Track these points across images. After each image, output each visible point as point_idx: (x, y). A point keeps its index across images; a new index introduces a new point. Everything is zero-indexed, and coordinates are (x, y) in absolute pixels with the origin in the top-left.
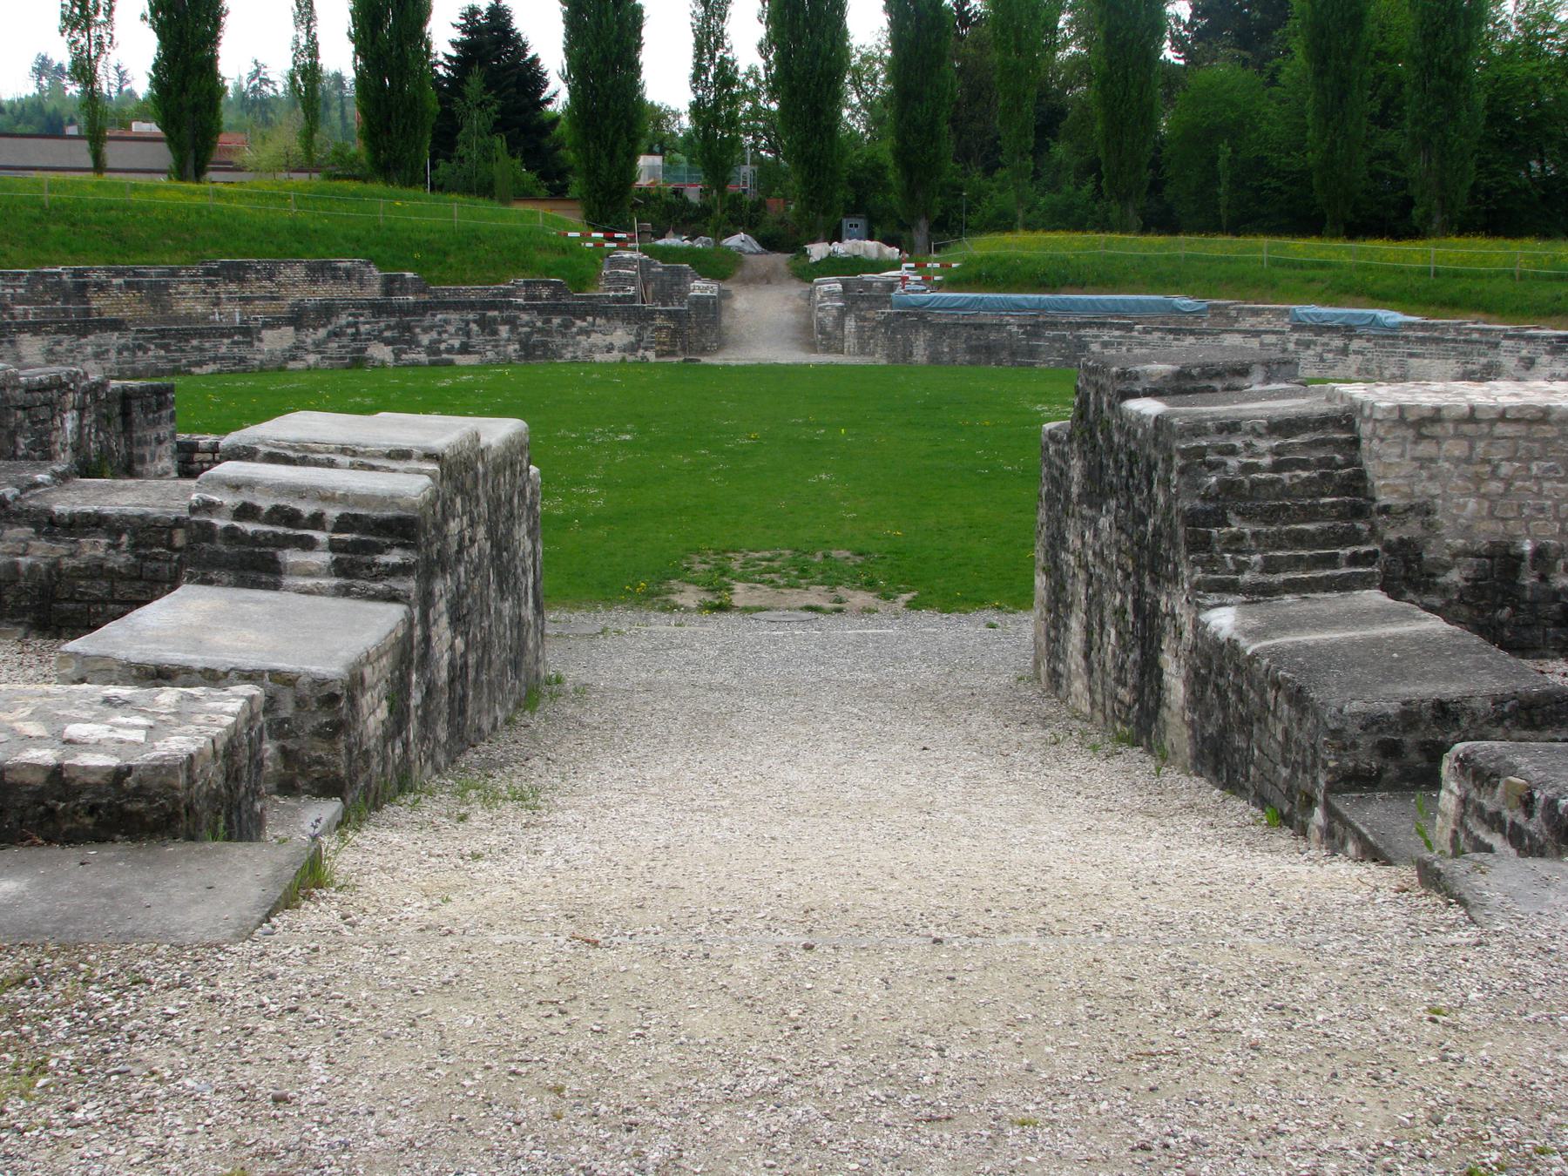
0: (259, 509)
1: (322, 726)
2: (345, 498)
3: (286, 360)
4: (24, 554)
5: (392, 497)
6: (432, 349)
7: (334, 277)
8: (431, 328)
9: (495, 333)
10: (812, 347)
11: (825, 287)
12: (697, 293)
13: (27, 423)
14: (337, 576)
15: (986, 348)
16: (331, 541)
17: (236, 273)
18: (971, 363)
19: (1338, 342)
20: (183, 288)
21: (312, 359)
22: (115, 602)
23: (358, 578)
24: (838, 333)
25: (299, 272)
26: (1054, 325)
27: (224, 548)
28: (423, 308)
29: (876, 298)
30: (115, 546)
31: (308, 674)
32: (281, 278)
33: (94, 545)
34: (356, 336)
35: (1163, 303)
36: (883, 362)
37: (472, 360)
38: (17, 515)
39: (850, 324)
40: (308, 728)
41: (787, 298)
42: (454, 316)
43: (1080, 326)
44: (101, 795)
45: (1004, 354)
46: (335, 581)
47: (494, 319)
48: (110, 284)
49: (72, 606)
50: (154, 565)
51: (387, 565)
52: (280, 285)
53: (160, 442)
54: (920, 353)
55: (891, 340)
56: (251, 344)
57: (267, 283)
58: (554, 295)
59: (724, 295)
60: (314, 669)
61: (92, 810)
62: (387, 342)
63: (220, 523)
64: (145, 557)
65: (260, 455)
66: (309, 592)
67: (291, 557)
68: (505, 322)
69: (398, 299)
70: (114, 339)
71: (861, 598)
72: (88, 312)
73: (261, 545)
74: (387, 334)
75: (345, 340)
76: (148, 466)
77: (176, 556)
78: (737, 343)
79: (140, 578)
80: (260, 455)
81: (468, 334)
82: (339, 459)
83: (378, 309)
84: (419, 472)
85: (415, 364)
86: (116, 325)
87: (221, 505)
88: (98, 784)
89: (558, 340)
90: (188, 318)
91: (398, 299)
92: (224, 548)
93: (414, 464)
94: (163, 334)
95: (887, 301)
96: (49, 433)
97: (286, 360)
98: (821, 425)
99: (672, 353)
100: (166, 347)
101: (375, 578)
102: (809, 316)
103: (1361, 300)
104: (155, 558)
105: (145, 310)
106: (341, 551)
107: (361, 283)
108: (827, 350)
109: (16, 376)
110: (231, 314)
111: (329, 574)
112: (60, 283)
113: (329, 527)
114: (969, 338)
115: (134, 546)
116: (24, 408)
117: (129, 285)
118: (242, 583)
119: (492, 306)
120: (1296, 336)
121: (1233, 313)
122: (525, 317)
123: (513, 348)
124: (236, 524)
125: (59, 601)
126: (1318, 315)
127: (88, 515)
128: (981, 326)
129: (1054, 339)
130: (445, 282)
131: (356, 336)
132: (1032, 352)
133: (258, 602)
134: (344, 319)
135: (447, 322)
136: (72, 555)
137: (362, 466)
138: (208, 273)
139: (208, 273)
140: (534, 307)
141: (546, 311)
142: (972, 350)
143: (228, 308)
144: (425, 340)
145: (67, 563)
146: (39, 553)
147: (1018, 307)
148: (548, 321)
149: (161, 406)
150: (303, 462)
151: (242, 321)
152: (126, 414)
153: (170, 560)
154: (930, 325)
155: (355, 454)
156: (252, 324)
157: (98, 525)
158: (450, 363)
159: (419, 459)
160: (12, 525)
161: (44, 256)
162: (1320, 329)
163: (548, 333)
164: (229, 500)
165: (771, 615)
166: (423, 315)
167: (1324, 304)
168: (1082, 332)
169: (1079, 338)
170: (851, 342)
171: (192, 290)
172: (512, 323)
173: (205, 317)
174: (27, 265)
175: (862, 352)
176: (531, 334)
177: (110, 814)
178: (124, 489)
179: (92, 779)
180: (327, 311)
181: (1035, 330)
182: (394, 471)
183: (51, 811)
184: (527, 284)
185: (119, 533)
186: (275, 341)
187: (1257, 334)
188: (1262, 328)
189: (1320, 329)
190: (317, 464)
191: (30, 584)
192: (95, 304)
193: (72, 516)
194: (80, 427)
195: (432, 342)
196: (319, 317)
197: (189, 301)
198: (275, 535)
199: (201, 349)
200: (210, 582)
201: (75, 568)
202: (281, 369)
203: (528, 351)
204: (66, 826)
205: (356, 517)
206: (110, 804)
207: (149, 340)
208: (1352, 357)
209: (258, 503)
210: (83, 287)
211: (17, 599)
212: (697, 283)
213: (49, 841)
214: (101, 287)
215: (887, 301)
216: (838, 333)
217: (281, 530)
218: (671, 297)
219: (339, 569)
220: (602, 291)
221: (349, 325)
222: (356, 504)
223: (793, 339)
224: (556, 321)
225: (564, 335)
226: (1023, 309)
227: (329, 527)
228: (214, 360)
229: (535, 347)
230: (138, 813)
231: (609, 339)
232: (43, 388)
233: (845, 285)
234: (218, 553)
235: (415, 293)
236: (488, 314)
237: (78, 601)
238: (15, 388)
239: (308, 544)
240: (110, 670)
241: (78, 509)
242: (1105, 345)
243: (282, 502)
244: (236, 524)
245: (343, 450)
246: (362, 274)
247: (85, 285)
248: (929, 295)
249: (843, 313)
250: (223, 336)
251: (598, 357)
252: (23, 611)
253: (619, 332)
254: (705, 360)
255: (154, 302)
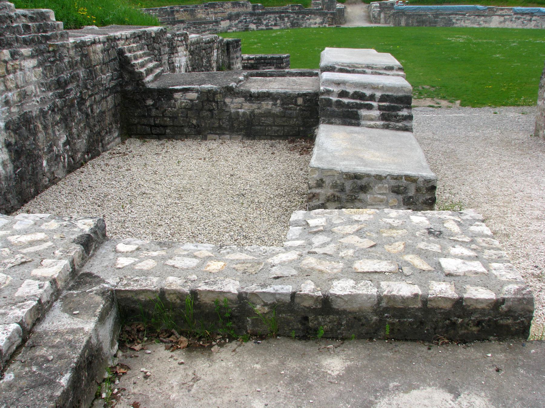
0: (349, 93)
1: (427, 200)
2: (383, 88)
3: (228, 29)
4: (241, 108)
5: (402, 87)
6: (267, 25)
7: (239, 6)
8: (266, 19)
9: (284, 20)
10: (371, 22)
11: (374, 5)
12: (338, 7)
13: (205, 55)
14: (382, 120)
15: (422, 21)
16: (379, 106)
17: (213, 6)
18: (417, 26)
19: (528, 18)
20: (199, 10)
21: (234, 29)
22: (275, 126)
23: (391, 121)
24: (379, 18)
25: (230, 5)
26: (442, 14)
27: (336, 109)
28: (263, 14)
29: (390, 8)
30: (275, 105)
31: (422, 177)
32: (225, 7)
33: (267, 104)
34: (246, 22)
35: (474, 7)
36: (392, 26)
37: (278, 28)
38: (238, 93)
39: (382, 15)
40: (421, 200)
41: (362, 8)
42: (272, 16)
43: (450, 14)
44: (485, 315)
45: (427, 23)
46: (382, 123)
47: (283, 16)
48: (180, 11)
49: (259, 128)
50: (290, 112)
51: (403, 116)
52: (225, 9)
53: (237, 58)
54: (403, 23)
55: (395, 20)
56: (218, 25)
57: (221, 8)
58: (299, 9)
59: (345, 8)
60: (424, 174)
61: (478, 323)
62: (254, 24)
63: (334, 99)
64: (286, 108)
65: (337, 69)
66: (372, 127)
67: (363, 112)
68: (286, 17)
69: (257, 11)
70: (182, 25)
71: (444, 103)
72: (174, 19)
73: (351, 108)
74: (254, 21)
75: (243, 24)
76: (234, 66)
77: (298, 108)
78: (350, 21)
79: (284, 117)
80: (337, 69)
81: (276, 21)
82: (367, 70)
83: (252, 14)
84: (398, 75)
85: (262, 30)
86: (182, 22)
87: (333, 91)
88: (483, 309)
89: (301, 22)
90: (201, 19)
91: (257, 11)
92: (336, 109)
93: (395, 72)
94: (195, 24)
95: (393, 8)
96: (211, 57)
97: (228, 29)
98: (390, 45)
99: (332, 25)
100: (196, 27)
101: (398, 121)
102: (369, 13)
103: (535, 4)
104: (290, 109)
105: (189, 17)
106: (383, 110)
107: (246, 7)
108: (375, 23)
109: (202, 39)
110: (212, 17)
111: (379, 120)
112: (167, 11)
113: (377, 100)
114: (417, 18)
115: (282, 105)
116: (204, 49)
117: (185, 10)
118: (345, 124)
119: (283, 12)
120: (515, 16)
121: (495, 10)
122: (292, 15)
123: (288, 24)
124: (340, 99)
125: (254, 126)
126: (521, 10)
127: (265, 93)
128: (421, 15)
129: (442, 18)
130: (269, 6)
131: (246, 22)
132: (436, 22)
133: (359, 133)
134: (242, 18)
135: (270, 17)
136: (259, 108)
137: (376, 73)
138: (205, 6)
139: (205, 6)
140: (294, 12)
141: (297, 13)
142: (418, 22)
143: (211, 16)
144: (265, 22)
145: (257, 111)
146: (246, 108)
147: (431, 9)
148: (298, 16)
149: (238, 46)
150: (353, 72)
151: (215, 19)
152: (228, 49)
153: (296, 110)
154: (406, 15)
155: (372, 68)
156: (218, 20)
157: (268, 97)
158: (271, 29)
159: (397, 70)
160: (236, 97)
161: (162, 4)
162: (523, 14)
163: (298, 20)
164: (336, 89)
165: (420, 109)
166: (264, 15)
167: (523, 6)
168: (450, 16)
169: (449, 18)
170: (382, 20)
171: (201, 11)
172: (288, 17)
173: (205, 18)
174: (158, 6)
175: (386, 23)
176: (293, 20)
177: (489, 326)
178: (270, 81)
179: (479, 306)
180: (238, 15)
181: (436, 16)
182: (388, 75)
183: (454, 324)
184: (292, 6)
185: (276, 99)
186: (224, 24)
187: (503, 16)
188: (504, 14)
189: (523, 14)
190: (359, 72)
191: (243, 119)
192: (176, 16)
193: (258, 93)
194: (218, 55)
195: (267, 23)
196: (236, 17)
197: (201, 14)
198: (357, 104)
199: (205, 27)
200: (332, 123)
201: (260, 113)
202: (226, 32)
203: (293, 25)
204: (462, 332)
205: (388, 96)
206: (489, 320)
207: (191, 25)
208: (533, 22)
209: (348, 90)
210: (172, 12)
211: (239, 125)
212: (338, 5)
213: (451, 340)
214: (178, 11)
215: (393, 8)
216: (379, 18)
217: (358, 101)
218: (330, 8)
219: (383, 117)
220: (312, 7)
221: (244, 19)
222: (387, 90)
223: (365, 20)
224: (301, 16)
225: (303, 20)
226: (432, 10)
227: (377, 100)
228: (208, 30)
229: (295, 24)
230: (507, 326)
231: (315, 21)
232: (209, 42)
233: (380, 4)
234: (334, 111)
235: (261, 9)
236: (282, 15)
237: (261, 126)
238: (202, 43)
239: (370, 107)
240: (334, 175)
241: (260, 90)
242: (457, 20)
243: (358, 90)
244: (340, 99)
245: (368, 67)
246: (247, 5)
247: (173, 11)
248: (405, 6)
249: (380, 12)
250: (210, 23)
251: (312, 26)
252: (241, 130)
253: (318, 19)
254: (342, 26)
255: (191, 15)
